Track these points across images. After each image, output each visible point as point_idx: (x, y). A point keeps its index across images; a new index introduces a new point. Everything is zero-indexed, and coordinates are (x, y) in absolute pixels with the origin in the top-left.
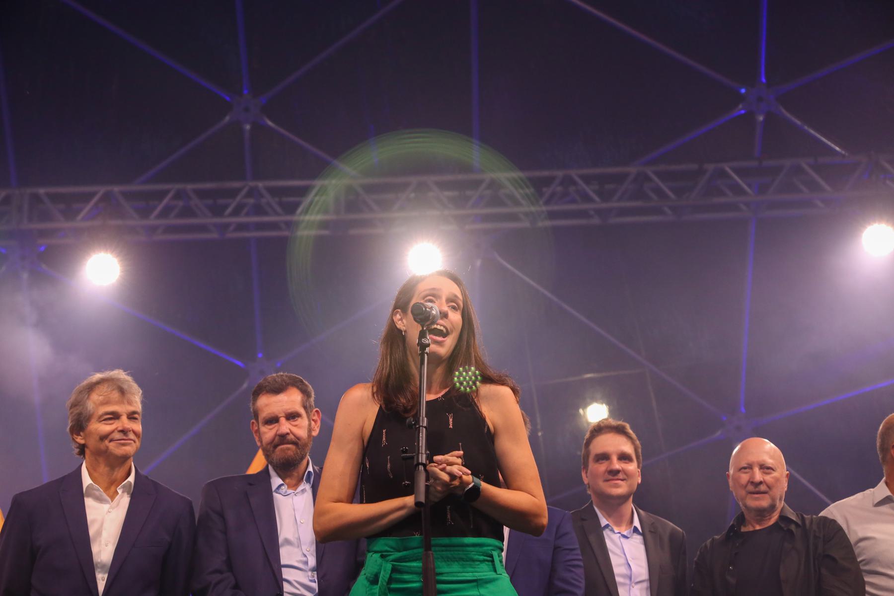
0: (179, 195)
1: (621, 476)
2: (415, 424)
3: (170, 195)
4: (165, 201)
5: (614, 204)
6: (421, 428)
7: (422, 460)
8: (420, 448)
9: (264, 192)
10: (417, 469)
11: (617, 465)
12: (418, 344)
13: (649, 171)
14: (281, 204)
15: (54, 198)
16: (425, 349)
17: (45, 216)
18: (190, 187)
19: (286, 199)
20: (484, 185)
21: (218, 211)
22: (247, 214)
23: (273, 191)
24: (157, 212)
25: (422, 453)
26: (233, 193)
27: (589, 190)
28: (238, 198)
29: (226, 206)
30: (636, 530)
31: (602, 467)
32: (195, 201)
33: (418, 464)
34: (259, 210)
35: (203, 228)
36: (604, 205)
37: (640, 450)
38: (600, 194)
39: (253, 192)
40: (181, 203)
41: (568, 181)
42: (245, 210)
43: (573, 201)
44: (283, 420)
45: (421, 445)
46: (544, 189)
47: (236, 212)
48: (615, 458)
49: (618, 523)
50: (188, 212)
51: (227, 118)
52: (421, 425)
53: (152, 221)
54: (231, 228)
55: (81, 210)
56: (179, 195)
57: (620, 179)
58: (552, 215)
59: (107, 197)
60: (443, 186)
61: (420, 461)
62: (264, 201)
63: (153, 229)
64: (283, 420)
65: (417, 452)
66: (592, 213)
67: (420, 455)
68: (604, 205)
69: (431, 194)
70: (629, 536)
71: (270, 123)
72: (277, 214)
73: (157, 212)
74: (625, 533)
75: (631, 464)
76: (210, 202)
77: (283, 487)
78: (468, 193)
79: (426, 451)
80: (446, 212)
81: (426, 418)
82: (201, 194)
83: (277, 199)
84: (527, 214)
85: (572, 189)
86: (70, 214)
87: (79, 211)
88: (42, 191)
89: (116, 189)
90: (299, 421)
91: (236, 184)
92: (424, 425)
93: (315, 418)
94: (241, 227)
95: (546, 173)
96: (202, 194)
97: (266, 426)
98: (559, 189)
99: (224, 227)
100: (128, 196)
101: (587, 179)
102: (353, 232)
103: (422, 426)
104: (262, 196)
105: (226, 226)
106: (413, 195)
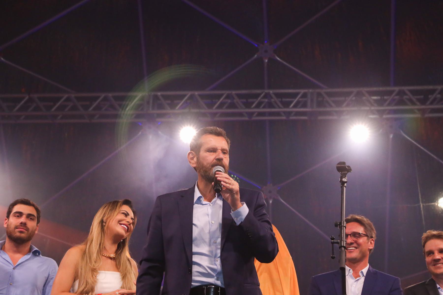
0: (228, 97)
2: (339, 225)
6: (343, 227)
7: (343, 245)
8: (342, 238)
9: (273, 96)
12: (340, 181)
14: (281, 102)
15: (166, 98)
16: (344, 184)
17: (161, 107)
18: (234, 92)
19: (284, 100)
20: (437, 92)
21: (248, 105)
22: (264, 107)
23: (278, 95)
25: (343, 241)
28: (259, 99)
29: (253, 103)
32: (236, 100)
34: (270, 105)
35: (241, 114)
39: (267, 96)
42: (263, 105)
43: (405, 104)
45: (342, 236)
46: (430, 96)
47: (258, 106)
50: (233, 106)
51: (256, 56)
52: (343, 225)
53: (214, 110)
54: (255, 115)
55: (178, 104)
56: (228, 97)
58: (223, 114)
59: (192, 97)
61: (342, 245)
62: (273, 100)
63: (214, 114)
64: (220, 151)
65: (340, 240)
67: (342, 242)
69: (364, 98)
71: (278, 59)
72: (280, 107)
76: (245, 100)
77: (201, 199)
78: (385, 97)
79: (345, 240)
80: (373, 108)
81: (345, 222)
82: (239, 96)
83: (280, 100)
85: (405, 97)
86: (173, 106)
87: (178, 104)
89: (196, 93)
92: (344, 226)
94: (260, 114)
95: (431, 87)
96: (240, 96)
97: (208, 153)
98: (439, 96)
102: (320, 118)
103: (343, 226)
104: (272, 98)
105: (252, 113)
106: (354, 98)
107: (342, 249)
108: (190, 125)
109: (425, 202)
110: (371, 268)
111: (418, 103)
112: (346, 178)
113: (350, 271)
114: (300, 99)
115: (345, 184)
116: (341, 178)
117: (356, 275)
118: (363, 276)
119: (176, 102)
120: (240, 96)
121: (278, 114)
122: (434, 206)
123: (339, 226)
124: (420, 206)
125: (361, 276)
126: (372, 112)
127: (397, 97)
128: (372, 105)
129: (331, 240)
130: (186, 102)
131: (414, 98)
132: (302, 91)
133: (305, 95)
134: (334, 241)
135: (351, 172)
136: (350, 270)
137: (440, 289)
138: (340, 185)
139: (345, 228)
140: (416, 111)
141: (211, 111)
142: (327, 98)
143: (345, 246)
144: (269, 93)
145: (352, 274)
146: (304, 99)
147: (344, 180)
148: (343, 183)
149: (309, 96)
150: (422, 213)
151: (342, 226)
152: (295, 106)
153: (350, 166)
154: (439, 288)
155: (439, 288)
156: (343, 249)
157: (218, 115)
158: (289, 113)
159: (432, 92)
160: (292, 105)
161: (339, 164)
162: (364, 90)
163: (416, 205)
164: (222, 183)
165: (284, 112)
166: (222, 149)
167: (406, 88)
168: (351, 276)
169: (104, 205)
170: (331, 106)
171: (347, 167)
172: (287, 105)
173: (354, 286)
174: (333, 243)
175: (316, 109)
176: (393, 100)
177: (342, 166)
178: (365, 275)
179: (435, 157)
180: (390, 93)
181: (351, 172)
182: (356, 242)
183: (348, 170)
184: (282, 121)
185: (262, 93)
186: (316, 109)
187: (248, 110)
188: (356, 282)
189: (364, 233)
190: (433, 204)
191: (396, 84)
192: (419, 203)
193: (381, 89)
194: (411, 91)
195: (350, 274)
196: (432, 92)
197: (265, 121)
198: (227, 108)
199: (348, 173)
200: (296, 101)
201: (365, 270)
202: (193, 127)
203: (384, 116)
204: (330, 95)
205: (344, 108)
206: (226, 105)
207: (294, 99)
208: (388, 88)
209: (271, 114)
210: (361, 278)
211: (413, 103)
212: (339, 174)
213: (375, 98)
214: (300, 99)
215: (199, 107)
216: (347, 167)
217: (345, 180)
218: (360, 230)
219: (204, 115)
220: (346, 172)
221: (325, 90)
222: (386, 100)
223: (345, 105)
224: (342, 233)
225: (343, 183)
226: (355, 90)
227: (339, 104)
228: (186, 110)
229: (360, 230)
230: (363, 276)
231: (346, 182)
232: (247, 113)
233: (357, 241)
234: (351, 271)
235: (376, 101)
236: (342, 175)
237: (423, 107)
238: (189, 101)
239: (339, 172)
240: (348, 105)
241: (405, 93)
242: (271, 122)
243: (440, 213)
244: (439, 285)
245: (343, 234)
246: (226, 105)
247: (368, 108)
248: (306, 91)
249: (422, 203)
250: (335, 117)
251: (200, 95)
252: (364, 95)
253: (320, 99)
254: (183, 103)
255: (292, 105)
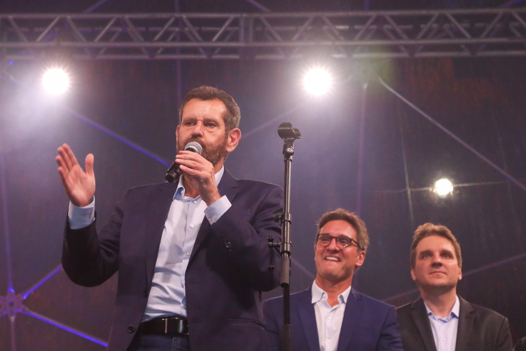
0: (118, 23)
1: (442, 269)
3: (111, 23)
4: (107, 28)
5: (482, 40)
6: (286, 222)
9: (188, 23)
10: (283, 256)
11: (439, 260)
13: (515, 12)
14: (200, 33)
15: (21, 23)
18: (127, 16)
20: (433, 19)
21: (148, 36)
22: (174, 40)
23: (195, 22)
24: (100, 36)
25: (287, 243)
26: (162, 22)
27: (461, 27)
28: (166, 27)
29: (156, 33)
30: (453, 315)
31: (428, 262)
32: (131, 28)
33: (284, 252)
34: (183, 37)
35: (137, 51)
36: (474, 41)
37: (460, 251)
38: (469, 30)
39: (178, 22)
40: (120, 30)
41: (443, 19)
42: (171, 37)
43: (447, 37)
44: (200, 123)
46: (422, 26)
47: (164, 38)
48: (437, 254)
49: (441, 311)
50: (125, 37)
53: (96, 43)
54: (160, 51)
56: (118, 23)
57: (489, 18)
59: (62, 23)
60: (336, 21)
61: (285, 249)
62: (186, 29)
63: (97, 50)
64: (200, 123)
65: (282, 242)
66: (463, 46)
67: (285, 244)
68: (474, 41)
69: (325, 28)
70: (446, 321)
72: (197, 41)
73: (100, 36)
74: (444, 319)
75: (451, 260)
76: (143, 29)
78: (357, 27)
80: (338, 43)
83: (197, 28)
84: (406, 47)
85: (446, 26)
86: (32, 36)
87: (40, 33)
88: (11, 17)
89: (69, 17)
90: (215, 129)
91: (164, 15)
92: (288, 220)
93: (235, 136)
95: (424, 12)
96: (136, 22)
98: (435, 26)
99: (153, 51)
100: (78, 23)
101: (459, 18)
102: (258, 57)
104: (185, 25)
105: (156, 49)
106: (310, 28)
107: (284, 255)
108: (59, 66)
109: (415, 187)
110: (354, 292)
111: (405, 36)
112: (292, 147)
113: (324, 295)
114: (229, 29)
115: (291, 157)
116: (285, 147)
117: (333, 303)
118: (343, 302)
119: (36, 30)
120: (136, 22)
121: (194, 50)
122: (427, 192)
123: (280, 221)
124: (406, 193)
125: (340, 302)
126: (337, 50)
127: (374, 27)
128: (337, 39)
129: (268, 241)
130: (52, 30)
131: (399, 29)
132: (232, 16)
133: (235, 23)
134: (272, 244)
135: (300, 138)
136: (323, 294)
137: (432, 316)
138: (282, 157)
139: (289, 223)
140: (403, 49)
141: (91, 44)
142: (269, 27)
143: (289, 251)
144: (181, 18)
145: (328, 299)
146: (236, 28)
147: (289, 150)
148: (287, 155)
149: (242, 23)
150: (410, 202)
151: (285, 221)
152: (220, 39)
153: (299, 130)
154: (430, 314)
155: (430, 314)
156: (286, 255)
157: (102, 52)
158: (212, 50)
159: (426, 19)
160: (216, 37)
161: (282, 126)
162: (325, 15)
163: (401, 191)
164: (182, 167)
165: (205, 48)
166: (205, 118)
167: (387, 14)
168: (325, 303)
169: (235, 108)
170: (275, 39)
171: (293, 131)
172: (207, 37)
173: (330, 318)
174: (271, 247)
175: (252, 44)
176: (368, 31)
177: (286, 130)
178: (346, 301)
179: (430, 118)
180: (363, 20)
181: (300, 138)
182: (341, 251)
183: (297, 136)
184: (201, 61)
185: (171, 18)
186: (252, 44)
187: (148, 44)
188: (333, 312)
189: (355, 240)
190: (426, 189)
191: (371, 8)
192: (404, 187)
193: (351, 14)
194: (394, 18)
195: (323, 299)
196: (426, 19)
197: (174, 61)
198: (117, 40)
199: (294, 139)
200: (222, 29)
201: (346, 294)
202: (63, 69)
203: (355, 56)
204: (274, 22)
205: (295, 43)
206: (115, 36)
207: (218, 29)
208: (361, 14)
209: (184, 50)
210: (340, 305)
211: (398, 37)
212: (281, 142)
213: (341, 27)
214: (229, 29)
215: (73, 39)
216: (293, 131)
217: (289, 150)
218: (348, 232)
219: (81, 51)
220: (293, 138)
221: (266, 14)
222: (357, 31)
223: (296, 36)
224: (286, 231)
225: (287, 155)
226: (312, 15)
227: (287, 36)
228: (53, 44)
229: (348, 232)
230: (343, 302)
231: (292, 154)
232: (147, 48)
233: (344, 250)
234: (326, 295)
235: (342, 32)
236: (286, 143)
237: (412, 42)
238: (57, 29)
239: (283, 139)
240: (301, 38)
241: (385, 22)
242: (184, 62)
243: (436, 202)
244: (431, 310)
245: (287, 232)
246: (115, 36)
247: (329, 43)
248: (238, 15)
249: (411, 187)
250: (280, 57)
251: (74, 20)
252: (324, 23)
253: (259, 28)
254: (49, 32)
255: (216, 37)
